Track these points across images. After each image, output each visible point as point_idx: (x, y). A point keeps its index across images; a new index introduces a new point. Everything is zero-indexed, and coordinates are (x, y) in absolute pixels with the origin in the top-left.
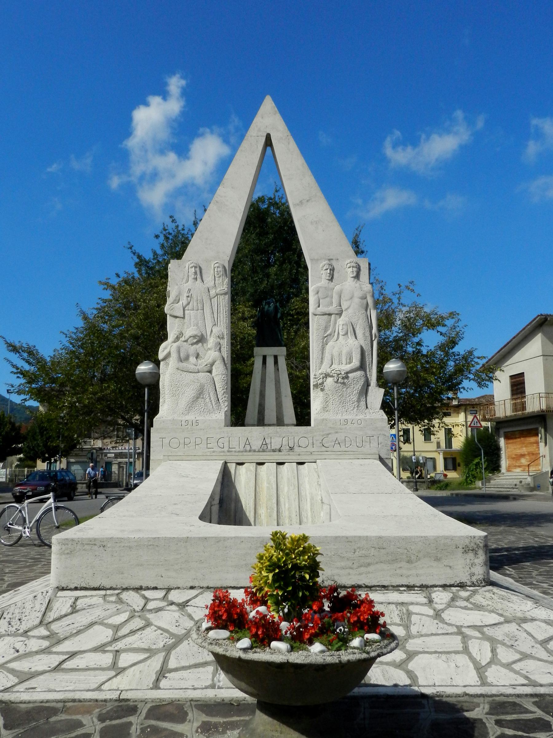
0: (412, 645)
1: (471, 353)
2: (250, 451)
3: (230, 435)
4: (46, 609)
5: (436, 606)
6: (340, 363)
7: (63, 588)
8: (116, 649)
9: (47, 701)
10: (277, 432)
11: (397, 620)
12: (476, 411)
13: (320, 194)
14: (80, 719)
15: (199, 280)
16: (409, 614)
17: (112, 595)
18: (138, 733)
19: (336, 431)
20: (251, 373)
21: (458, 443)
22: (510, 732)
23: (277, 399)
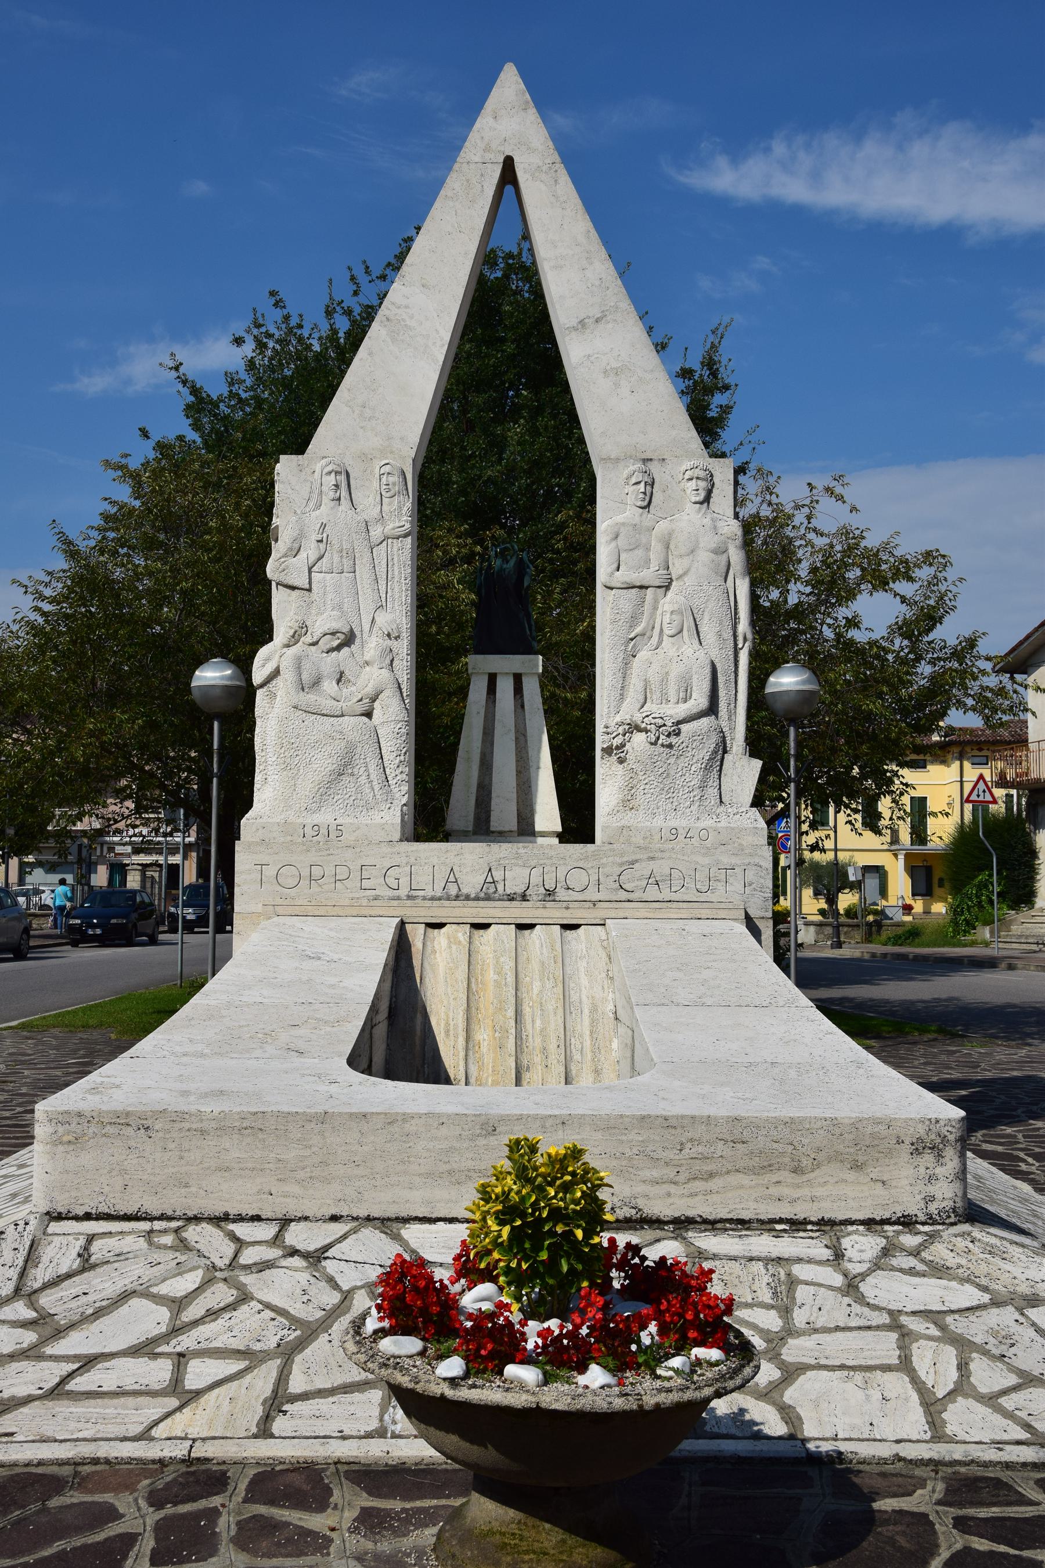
0: (794, 1351)
1: (971, 643)
2: (457, 897)
3: (412, 860)
4: (26, 1261)
5: (849, 1266)
6: (665, 700)
7: (60, 1213)
8: (179, 1349)
9: (41, 1463)
10: (518, 856)
11: (766, 1297)
12: (987, 757)
13: (626, 304)
14: (111, 1501)
15: (345, 502)
16: (793, 1282)
17: (165, 1231)
18: (233, 1533)
19: (652, 855)
20: (463, 692)
21: (941, 830)
22: (981, 1545)
23: (519, 773)
